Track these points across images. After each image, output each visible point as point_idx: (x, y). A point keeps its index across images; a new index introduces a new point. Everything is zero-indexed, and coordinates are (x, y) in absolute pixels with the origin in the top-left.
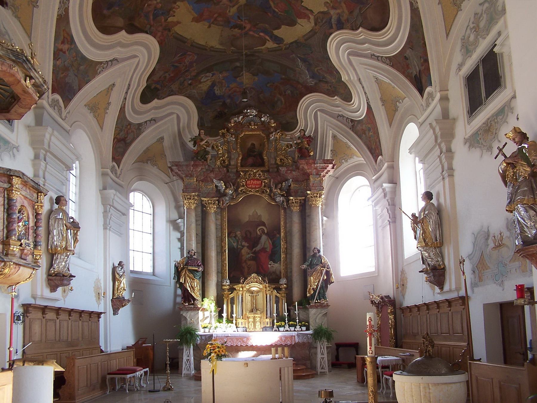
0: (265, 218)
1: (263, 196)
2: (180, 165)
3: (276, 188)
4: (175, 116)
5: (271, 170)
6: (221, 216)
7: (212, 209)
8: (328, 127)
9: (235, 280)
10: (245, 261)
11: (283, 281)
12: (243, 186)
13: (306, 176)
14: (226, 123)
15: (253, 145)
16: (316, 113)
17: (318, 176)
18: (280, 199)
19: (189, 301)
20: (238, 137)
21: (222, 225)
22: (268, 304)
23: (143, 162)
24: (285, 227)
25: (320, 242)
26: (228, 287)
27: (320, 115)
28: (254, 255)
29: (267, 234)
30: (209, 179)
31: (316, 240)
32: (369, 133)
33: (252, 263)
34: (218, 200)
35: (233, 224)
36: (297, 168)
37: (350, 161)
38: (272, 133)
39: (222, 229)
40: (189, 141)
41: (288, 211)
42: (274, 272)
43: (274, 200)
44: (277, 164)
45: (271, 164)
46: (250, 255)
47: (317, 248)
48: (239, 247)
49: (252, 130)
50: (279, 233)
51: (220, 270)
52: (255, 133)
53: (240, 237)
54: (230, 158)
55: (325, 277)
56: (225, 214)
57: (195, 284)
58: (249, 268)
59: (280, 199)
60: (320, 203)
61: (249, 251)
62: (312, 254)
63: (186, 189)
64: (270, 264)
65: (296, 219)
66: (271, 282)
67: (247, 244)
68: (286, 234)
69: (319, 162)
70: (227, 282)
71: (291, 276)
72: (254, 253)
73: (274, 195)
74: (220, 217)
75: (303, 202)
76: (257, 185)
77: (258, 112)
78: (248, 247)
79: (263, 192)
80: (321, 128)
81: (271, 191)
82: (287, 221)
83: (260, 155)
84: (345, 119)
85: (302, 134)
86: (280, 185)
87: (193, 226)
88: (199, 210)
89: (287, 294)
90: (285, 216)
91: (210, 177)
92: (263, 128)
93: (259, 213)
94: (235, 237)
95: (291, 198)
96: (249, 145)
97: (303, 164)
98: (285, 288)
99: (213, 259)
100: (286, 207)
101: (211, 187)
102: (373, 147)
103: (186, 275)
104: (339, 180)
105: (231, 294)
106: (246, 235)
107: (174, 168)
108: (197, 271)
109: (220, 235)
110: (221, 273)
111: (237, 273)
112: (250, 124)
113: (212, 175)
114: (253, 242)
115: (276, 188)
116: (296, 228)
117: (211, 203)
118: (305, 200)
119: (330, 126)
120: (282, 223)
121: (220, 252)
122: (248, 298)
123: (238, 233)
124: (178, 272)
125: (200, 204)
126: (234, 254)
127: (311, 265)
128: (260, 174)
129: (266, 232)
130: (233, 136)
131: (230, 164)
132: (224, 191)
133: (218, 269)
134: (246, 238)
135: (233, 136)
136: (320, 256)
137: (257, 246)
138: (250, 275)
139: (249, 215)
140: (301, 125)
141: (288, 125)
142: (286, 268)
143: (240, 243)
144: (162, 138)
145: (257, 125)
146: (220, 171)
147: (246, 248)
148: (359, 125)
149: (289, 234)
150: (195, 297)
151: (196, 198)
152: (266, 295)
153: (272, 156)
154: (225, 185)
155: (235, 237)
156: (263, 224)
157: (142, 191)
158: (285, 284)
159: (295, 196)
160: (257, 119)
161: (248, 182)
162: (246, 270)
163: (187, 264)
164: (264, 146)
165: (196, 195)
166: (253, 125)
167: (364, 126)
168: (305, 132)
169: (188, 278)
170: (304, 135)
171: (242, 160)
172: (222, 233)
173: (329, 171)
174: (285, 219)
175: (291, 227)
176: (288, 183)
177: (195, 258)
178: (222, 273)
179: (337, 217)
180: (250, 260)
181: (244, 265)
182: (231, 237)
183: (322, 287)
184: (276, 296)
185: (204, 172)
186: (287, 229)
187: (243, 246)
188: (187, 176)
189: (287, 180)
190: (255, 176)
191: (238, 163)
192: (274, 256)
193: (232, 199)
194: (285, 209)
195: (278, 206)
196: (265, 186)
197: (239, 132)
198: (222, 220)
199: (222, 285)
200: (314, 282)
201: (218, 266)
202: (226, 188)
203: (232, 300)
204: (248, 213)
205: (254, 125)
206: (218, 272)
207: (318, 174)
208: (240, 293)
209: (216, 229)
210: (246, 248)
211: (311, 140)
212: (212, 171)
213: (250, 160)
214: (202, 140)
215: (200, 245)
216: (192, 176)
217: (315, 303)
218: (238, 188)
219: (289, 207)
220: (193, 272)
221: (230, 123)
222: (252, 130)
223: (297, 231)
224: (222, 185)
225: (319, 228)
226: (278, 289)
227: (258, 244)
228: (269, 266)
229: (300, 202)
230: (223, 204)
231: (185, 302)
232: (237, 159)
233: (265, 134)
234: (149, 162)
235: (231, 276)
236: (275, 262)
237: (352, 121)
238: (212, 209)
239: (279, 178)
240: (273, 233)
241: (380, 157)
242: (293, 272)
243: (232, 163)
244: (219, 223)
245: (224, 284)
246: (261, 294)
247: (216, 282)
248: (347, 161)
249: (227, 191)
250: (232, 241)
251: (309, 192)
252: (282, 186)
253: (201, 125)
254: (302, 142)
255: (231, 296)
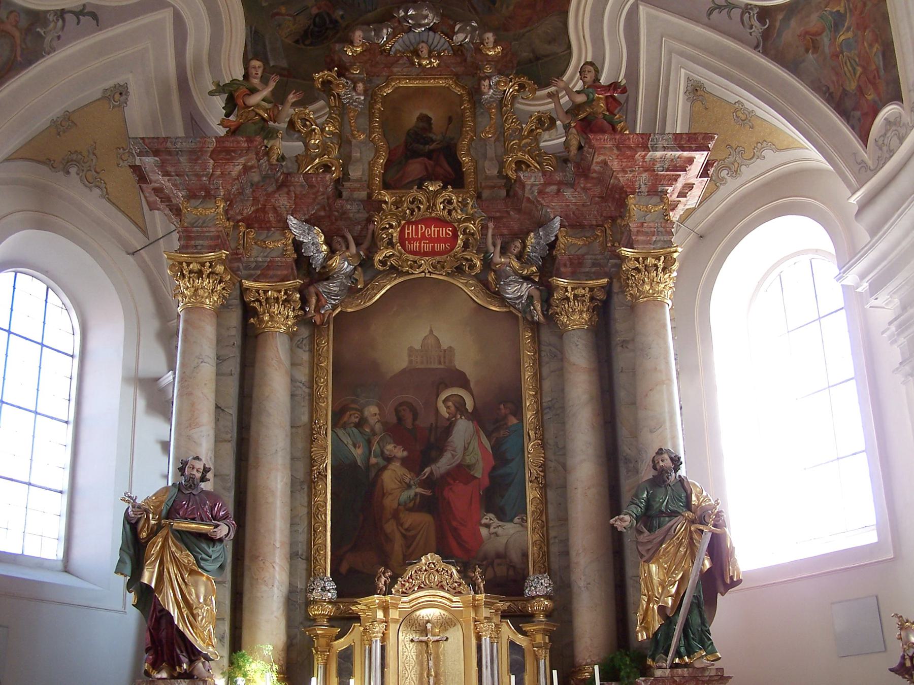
0: (466, 359)
1: (459, 282)
2: (169, 153)
3: (504, 252)
4: (166, 15)
5: (486, 194)
6: (311, 351)
7: (280, 321)
8: (675, 58)
9: (354, 583)
10: (396, 515)
11: (539, 586)
12: (391, 244)
13: (617, 197)
14: (338, 47)
15: (425, 119)
16: (633, 13)
17: (656, 199)
18: (516, 290)
19: (173, 663)
20: (374, 95)
21: (312, 382)
22: (486, 673)
23: (49, 163)
24: (539, 391)
25: (671, 422)
26: (329, 609)
27: (648, 15)
28: (427, 493)
29: (476, 416)
30: (271, 216)
31: (661, 425)
32: (833, 40)
33: (424, 519)
34: (301, 290)
35: (352, 379)
36: (583, 171)
37: (758, 166)
38: (489, 78)
39: (313, 399)
40: (211, 93)
41: (546, 336)
42: (501, 556)
43: (498, 296)
44: (507, 177)
45: (487, 178)
46: (412, 493)
47: (668, 451)
48: (373, 460)
49: (425, 73)
50: (518, 411)
51: (301, 549)
52: (432, 83)
53: (378, 427)
54: (347, 161)
55: (707, 564)
56: (327, 345)
57: (202, 590)
58: (408, 540)
59: (516, 290)
60: (666, 287)
61: (408, 476)
62: (647, 473)
63: (189, 238)
64: (488, 526)
65: (579, 356)
66: (495, 587)
67: (400, 453)
68: (540, 412)
69: (661, 144)
70: (326, 591)
71: (567, 568)
72: (428, 483)
73: (498, 279)
74: (305, 356)
75: (601, 296)
76: (439, 240)
77: (443, 16)
78: (405, 462)
79: (459, 270)
80: (648, 62)
81: (488, 264)
82: (545, 371)
83: (450, 152)
84: (736, 13)
85: (590, 77)
86: (518, 244)
87: (208, 370)
88: (234, 318)
89: (552, 636)
90: (538, 351)
91: (275, 209)
92: (459, 69)
93: (445, 343)
94: (358, 425)
95: (562, 282)
96: (411, 119)
97: (605, 154)
98: (549, 615)
99: (278, 503)
100: (545, 325)
101: (277, 244)
102: (852, 86)
103: (168, 557)
104: (718, 236)
105: (338, 637)
106: (400, 419)
107: (149, 162)
108: (211, 540)
109: (305, 418)
110: (302, 557)
111: (363, 550)
112: (416, 53)
113: (283, 201)
114: (424, 444)
115: (504, 252)
116: (580, 388)
117: (277, 300)
118: (608, 290)
119: (682, 54)
120: (527, 375)
121: (305, 482)
122: (405, 647)
123: (371, 411)
124: (136, 544)
125: (237, 302)
126: (356, 491)
127: (650, 518)
128: (450, 202)
129: (469, 406)
130: (360, 86)
131: (345, 176)
132: (323, 267)
133: (293, 544)
134: (397, 430)
135: (360, 86)
136: (681, 480)
137: (435, 460)
138: (411, 557)
139: (411, 350)
140: (581, 51)
141: (540, 65)
142: (545, 541)
143: (375, 447)
144: (122, 91)
145: (438, 57)
146: (311, 186)
147: (396, 466)
148: (793, 23)
149: (554, 411)
150: (199, 644)
151: (220, 268)
152: (479, 638)
153: (491, 152)
154: (327, 242)
155: (358, 425)
156: (461, 380)
157: (46, 273)
158: (547, 597)
159: (573, 275)
160: (438, 40)
161: (410, 231)
162: (398, 545)
163: (172, 513)
164: (462, 125)
165: (220, 261)
166: (425, 53)
167: (814, 17)
168: (598, 72)
169: (173, 570)
170: (597, 79)
171: (387, 166)
172: (313, 411)
173: (690, 186)
174: (538, 363)
175: (561, 391)
176: (547, 235)
177: (207, 493)
178: (308, 559)
179: (708, 365)
180: (411, 510)
181: (390, 527)
182: (344, 427)
183: (696, 604)
184: (512, 644)
185: (255, 186)
186: (546, 399)
187: (389, 460)
188: (192, 195)
189: (542, 223)
190: (431, 207)
191: (371, 176)
192: (500, 495)
193: (352, 291)
194: (535, 327)
195: (515, 316)
196: (466, 245)
197: (377, 81)
198: (314, 366)
199: (308, 603)
200: (660, 582)
201: (293, 524)
202: (332, 252)
203: (346, 657)
204: (406, 342)
205: (429, 57)
206: (293, 556)
207: (656, 192)
208: (379, 628)
209: (293, 396)
210: (396, 466)
211: (618, 95)
212: (284, 184)
213: (415, 168)
214: (253, 91)
215: (229, 450)
216: (209, 195)
217: (674, 666)
218: (373, 249)
219: (551, 318)
220: (195, 541)
221: (352, 43)
222: (425, 73)
223: (584, 398)
224: (316, 242)
225: (670, 379)
226: (519, 618)
227: (441, 451)
228: (484, 531)
229: (592, 299)
230: (317, 310)
231: (156, 666)
232: (371, 165)
233: (463, 88)
234: (73, 170)
235: (344, 568)
236: (502, 516)
237: (765, 13)
238: (280, 321)
239: (515, 221)
240: (497, 413)
241: (889, 110)
242: (573, 553)
243: (356, 172)
244: (302, 375)
245: (316, 595)
246: (455, 636)
247: (284, 589)
248: (736, 173)
249: (336, 262)
250: (347, 440)
251: (626, 252)
252: (524, 246)
253: (255, 48)
254: (590, 102)
255: (341, 644)
